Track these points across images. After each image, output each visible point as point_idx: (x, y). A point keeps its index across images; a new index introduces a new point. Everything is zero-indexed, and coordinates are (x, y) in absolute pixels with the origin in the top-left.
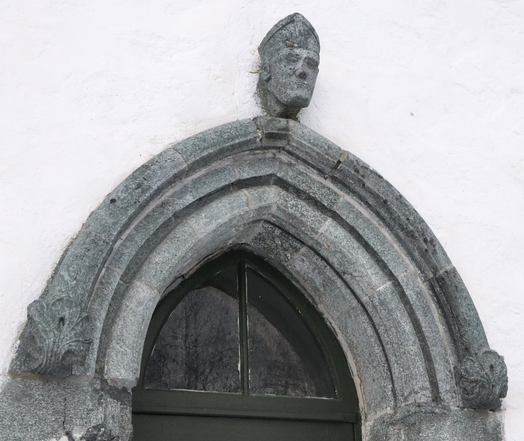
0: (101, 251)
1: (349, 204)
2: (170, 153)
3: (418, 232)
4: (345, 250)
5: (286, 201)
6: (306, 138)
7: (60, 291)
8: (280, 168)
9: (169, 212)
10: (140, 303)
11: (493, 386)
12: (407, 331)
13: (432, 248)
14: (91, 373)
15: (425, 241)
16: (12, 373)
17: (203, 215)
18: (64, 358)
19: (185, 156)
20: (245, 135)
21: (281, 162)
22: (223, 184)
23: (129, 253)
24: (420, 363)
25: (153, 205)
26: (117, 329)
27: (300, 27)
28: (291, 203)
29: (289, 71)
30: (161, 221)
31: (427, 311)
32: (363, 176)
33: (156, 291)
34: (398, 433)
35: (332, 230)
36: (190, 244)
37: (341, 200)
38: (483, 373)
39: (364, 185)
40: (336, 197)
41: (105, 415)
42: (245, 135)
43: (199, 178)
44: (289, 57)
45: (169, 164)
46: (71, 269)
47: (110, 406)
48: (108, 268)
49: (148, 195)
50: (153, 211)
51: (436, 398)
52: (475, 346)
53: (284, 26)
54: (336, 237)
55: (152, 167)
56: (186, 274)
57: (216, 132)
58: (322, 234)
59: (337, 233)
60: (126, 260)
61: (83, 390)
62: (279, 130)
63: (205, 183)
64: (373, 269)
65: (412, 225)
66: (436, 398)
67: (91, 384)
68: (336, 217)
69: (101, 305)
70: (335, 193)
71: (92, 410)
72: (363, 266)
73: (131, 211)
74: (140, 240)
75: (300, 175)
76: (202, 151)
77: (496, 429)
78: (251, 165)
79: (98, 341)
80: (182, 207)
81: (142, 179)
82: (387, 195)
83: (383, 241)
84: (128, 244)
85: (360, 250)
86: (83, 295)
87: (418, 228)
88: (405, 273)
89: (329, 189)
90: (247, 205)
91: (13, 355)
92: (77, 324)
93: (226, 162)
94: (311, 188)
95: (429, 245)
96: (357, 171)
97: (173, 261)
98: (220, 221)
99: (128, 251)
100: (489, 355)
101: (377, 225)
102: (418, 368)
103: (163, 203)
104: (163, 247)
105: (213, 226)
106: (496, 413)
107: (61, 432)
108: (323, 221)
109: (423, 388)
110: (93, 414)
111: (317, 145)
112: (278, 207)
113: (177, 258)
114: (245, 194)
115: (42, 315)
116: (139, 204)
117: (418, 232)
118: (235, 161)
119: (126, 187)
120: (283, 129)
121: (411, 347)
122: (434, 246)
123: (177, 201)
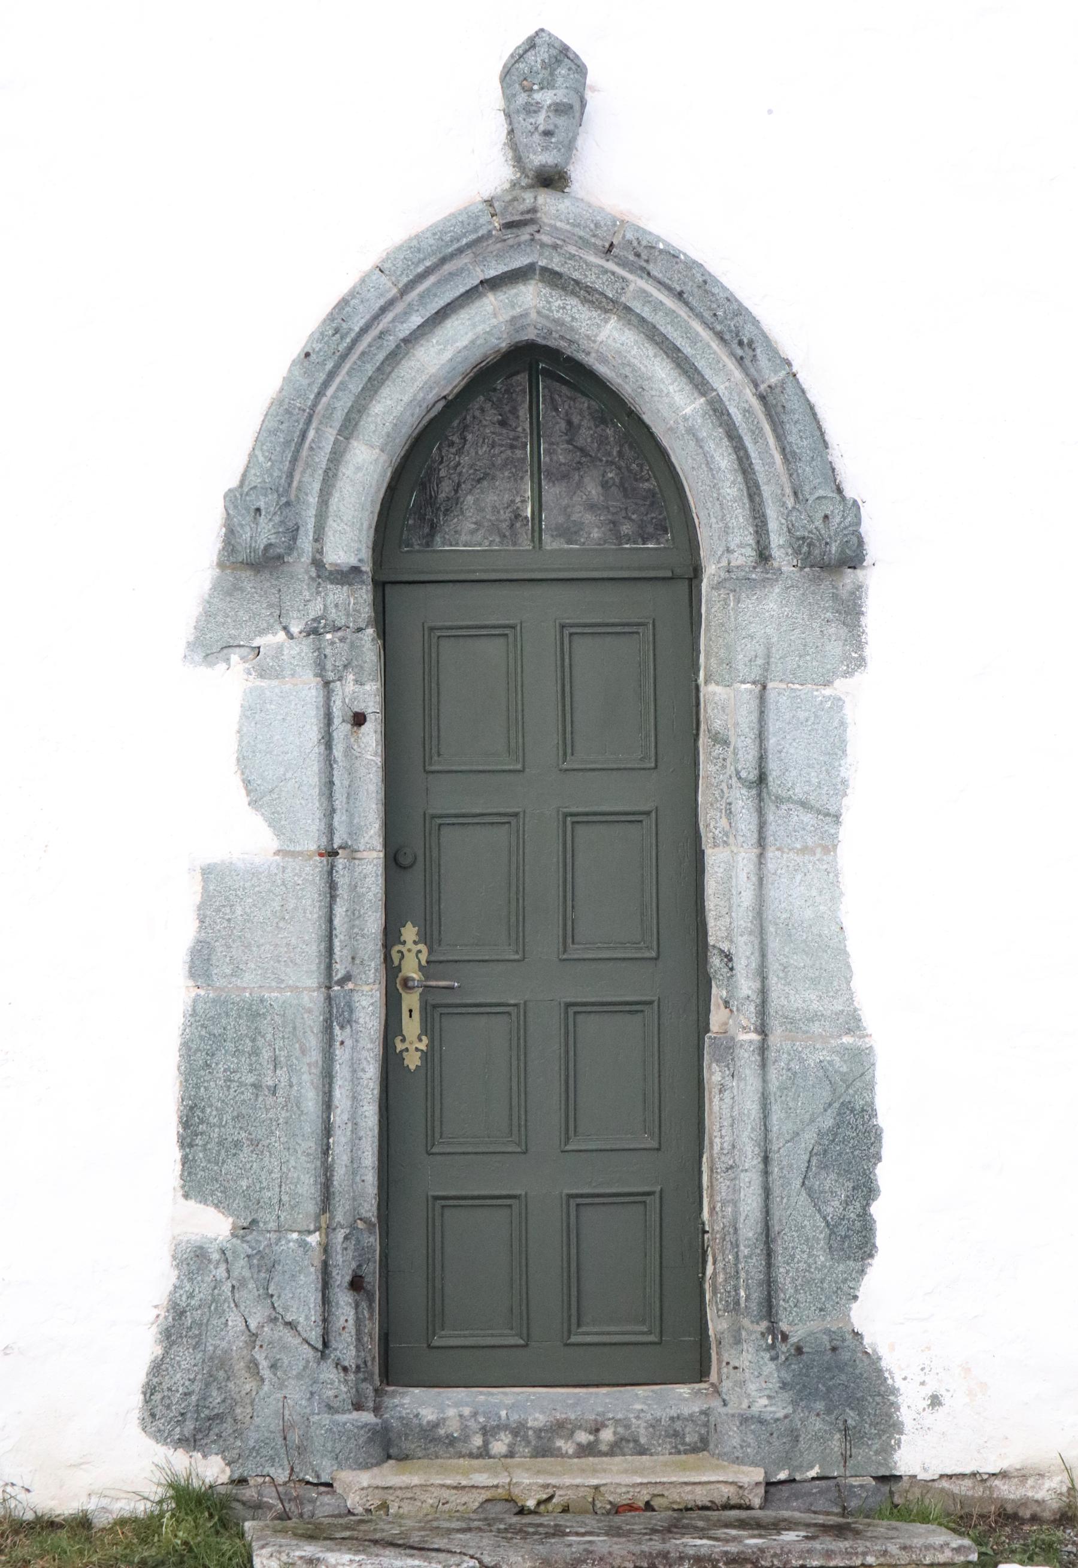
0: (297, 421)
1: (644, 291)
2: (374, 278)
3: (731, 331)
4: (636, 362)
5: (549, 302)
6: (563, 217)
7: (255, 475)
8: (541, 254)
9: (391, 342)
10: (359, 469)
11: (827, 543)
12: (723, 468)
13: (751, 353)
14: (306, 559)
15: (741, 343)
16: (221, 565)
17: (434, 341)
18: (264, 555)
19: (393, 279)
20: (476, 230)
21: (543, 245)
22: (462, 290)
23: (344, 403)
24: (740, 511)
25: (368, 339)
26: (334, 501)
27: (542, 54)
28: (557, 304)
29: (530, 127)
30: (381, 356)
31: (757, 434)
32: (647, 261)
33: (377, 451)
34: (725, 600)
35: (616, 334)
36: (419, 383)
37: (632, 287)
38: (812, 527)
39: (649, 274)
40: (624, 284)
41: (325, 605)
42: (476, 230)
43: (428, 290)
44: (545, 84)
45: (372, 295)
46: (265, 447)
47: (331, 594)
48: (317, 430)
49: (348, 340)
50: (370, 346)
51: (763, 556)
52: (807, 488)
53: (521, 56)
54: (622, 345)
55: (352, 302)
56: (448, 395)
57: (434, 234)
58: (601, 342)
59: (624, 338)
60: (339, 416)
61: (298, 579)
62: (522, 213)
63: (435, 295)
64: (676, 384)
65: (721, 323)
66: (763, 556)
67: (307, 572)
68: (626, 312)
69: (312, 476)
70: (623, 278)
71: (309, 601)
72: (662, 381)
73: (329, 365)
74: (356, 386)
75: (570, 259)
76: (417, 265)
77: (854, 593)
78: (499, 256)
79: (313, 520)
80: (408, 332)
81: (339, 320)
82: (684, 283)
83: (694, 340)
84: (340, 394)
85: (658, 359)
86: (280, 477)
87: (729, 326)
88: (727, 384)
89: (613, 273)
90: (495, 315)
91: (219, 545)
92: (275, 513)
93: (465, 260)
94: (586, 276)
95: (746, 348)
96: (638, 255)
97: (399, 408)
98: (458, 344)
99: (341, 403)
100: (824, 501)
101: (686, 318)
102: (736, 517)
103: (382, 333)
104: (385, 391)
105: (448, 355)
106: (858, 571)
107: (278, 627)
108: (603, 324)
109: (741, 546)
110: (310, 606)
111: (579, 225)
112: (538, 313)
113: (402, 403)
114: (490, 301)
115: (241, 503)
116: (338, 354)
117: (731, 331)
118: (476, 255)
119: (322, 334)
120: (528, 212)
121: (728, 490)
122: (754, 350)
123: (400, 327)
